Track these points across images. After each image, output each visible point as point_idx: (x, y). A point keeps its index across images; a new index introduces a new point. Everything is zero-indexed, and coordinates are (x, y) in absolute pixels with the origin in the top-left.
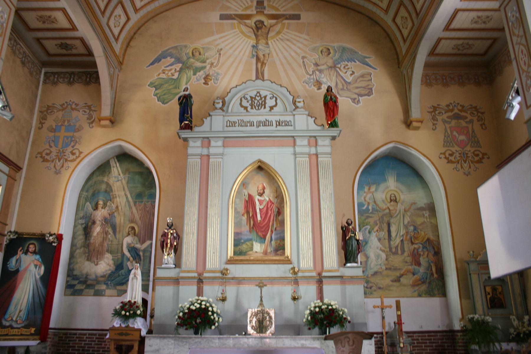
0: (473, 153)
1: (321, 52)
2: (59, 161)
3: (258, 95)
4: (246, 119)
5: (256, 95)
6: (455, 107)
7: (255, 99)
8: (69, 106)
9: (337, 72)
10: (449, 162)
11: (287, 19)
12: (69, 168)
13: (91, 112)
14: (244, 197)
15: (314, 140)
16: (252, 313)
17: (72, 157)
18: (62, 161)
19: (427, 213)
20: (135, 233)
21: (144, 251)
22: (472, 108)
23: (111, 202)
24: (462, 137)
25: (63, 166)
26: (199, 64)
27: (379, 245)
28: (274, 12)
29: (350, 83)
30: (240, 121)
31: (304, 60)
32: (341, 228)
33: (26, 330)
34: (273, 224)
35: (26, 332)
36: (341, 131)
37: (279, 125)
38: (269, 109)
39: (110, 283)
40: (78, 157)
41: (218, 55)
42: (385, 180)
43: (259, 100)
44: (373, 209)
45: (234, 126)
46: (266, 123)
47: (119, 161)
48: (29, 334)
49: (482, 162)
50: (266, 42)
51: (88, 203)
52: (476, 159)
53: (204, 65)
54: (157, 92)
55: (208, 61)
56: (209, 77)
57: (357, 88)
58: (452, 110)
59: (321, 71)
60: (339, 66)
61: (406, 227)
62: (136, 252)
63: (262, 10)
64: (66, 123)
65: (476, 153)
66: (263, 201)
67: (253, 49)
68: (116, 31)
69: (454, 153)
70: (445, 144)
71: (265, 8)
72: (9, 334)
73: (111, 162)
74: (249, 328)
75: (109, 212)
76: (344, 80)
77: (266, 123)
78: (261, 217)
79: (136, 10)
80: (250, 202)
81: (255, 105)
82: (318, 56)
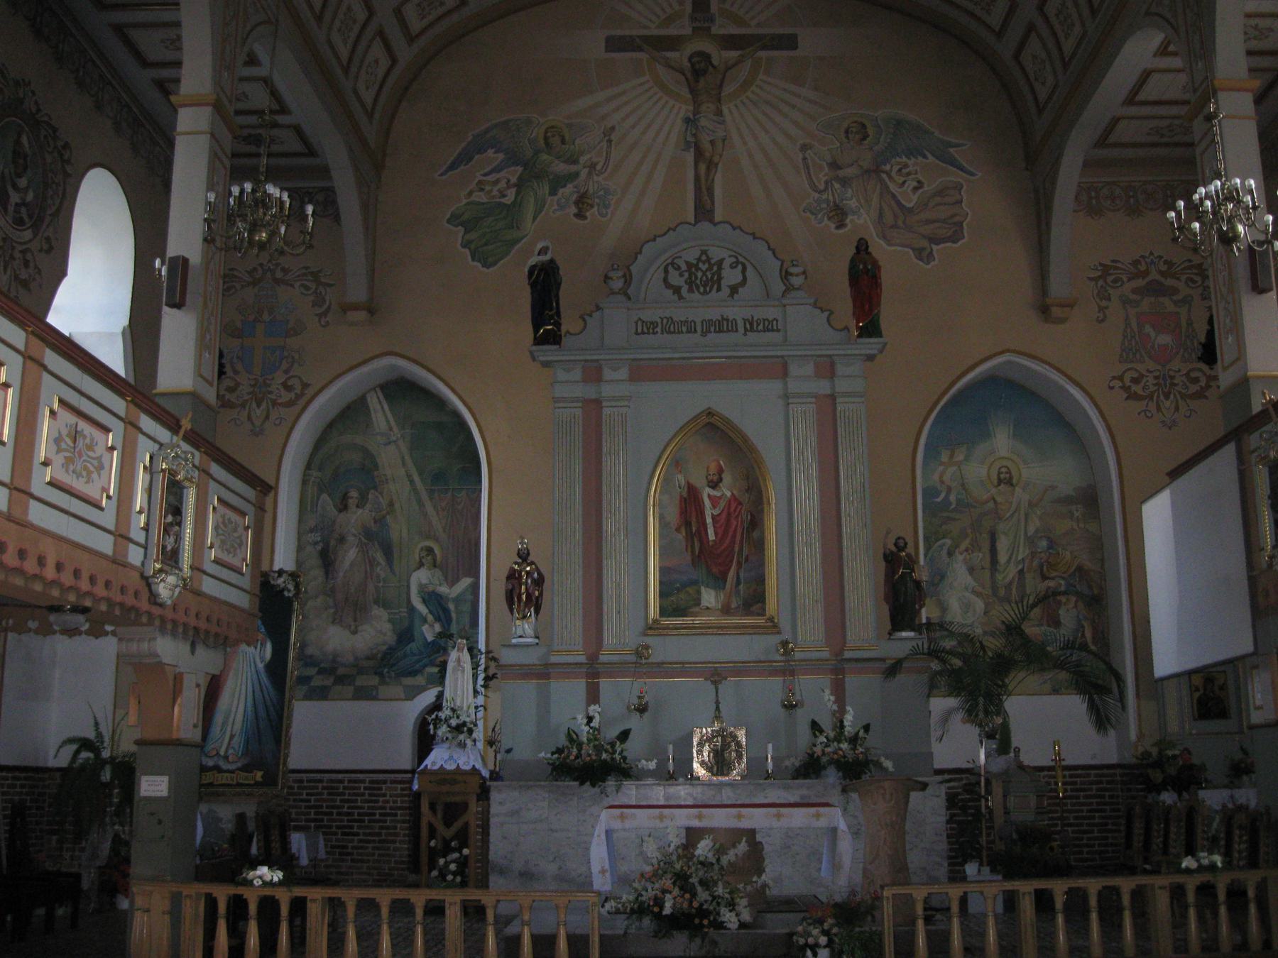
0: (1187, 375)
1: (847, 132)
2: (259, 406)
3: (704, 258)
4: (679, 314)
5: (699, 260)
6: (1153, 266)
7: (698, 269)
8: (269, 274)
9: (882, 182)
10: (1133, 396)
11: (764, 48)
12: (283, 421)
13: (321, 289)
14: (679, 490)
15: (827, 369)
16: (703, 736)
17: (286, 397)
18: (264, 405)
19: (1078, 511)
20: (435, 560)
21: (457, 600)
22: (1190, 268)
23: (377, 494)
24: (1165, 339)
25: (267, 417)
26: (560, 168)
27: (969, 580)
28: (733, 30)
29: (910, 210)
30: (665, 321)
31: (807, 156)
32: (882, 557)
33: (246, 774)
34: (741, 550)
35: (247, 778)
36: (886, 344)
37: (752, 330)
38: (728, 291)
39: (388, 672)
40: (301, 397)
41: (604, 144)
42: (986, 435)
43: (707, 270)
44: (958, 501)
45: (654, 333)
46: (723, 325)
47: (387, 397)
48: (252, 782)
49: (1206, 397)
50: (718, 108)
51: (325, 496)
52: (1194, 388)
53: (573, 168)
54: (473, 236)
55: (583, 160)
56: (585, 200)
57: (928, 222)
58: (1145, 274)
59: (845, 182)
60: (888, 167)
61: (1031, 541)
62: (440, 604)
63: (706, 25)
64: (266, 317)
65: (1193, 375)
66: (720, 498)
67: (687, 127)
68: (368, 97)
69: (1143, 376)
70: (1124, 354)
71: (712, 20)
72: (216, 783)
73: (369, 399)
74: (696, 765)
75: (373, 514)
76: (899, 203)
77: (723, 325)
78: (716, 534)
79: (411, 39)
80: (690, 502)
81: (698, 282)
82: (839, 145)
